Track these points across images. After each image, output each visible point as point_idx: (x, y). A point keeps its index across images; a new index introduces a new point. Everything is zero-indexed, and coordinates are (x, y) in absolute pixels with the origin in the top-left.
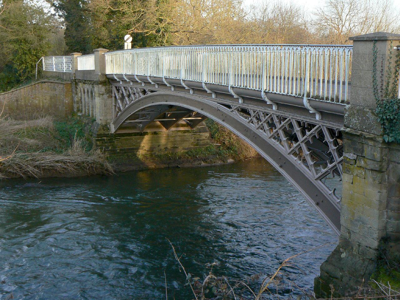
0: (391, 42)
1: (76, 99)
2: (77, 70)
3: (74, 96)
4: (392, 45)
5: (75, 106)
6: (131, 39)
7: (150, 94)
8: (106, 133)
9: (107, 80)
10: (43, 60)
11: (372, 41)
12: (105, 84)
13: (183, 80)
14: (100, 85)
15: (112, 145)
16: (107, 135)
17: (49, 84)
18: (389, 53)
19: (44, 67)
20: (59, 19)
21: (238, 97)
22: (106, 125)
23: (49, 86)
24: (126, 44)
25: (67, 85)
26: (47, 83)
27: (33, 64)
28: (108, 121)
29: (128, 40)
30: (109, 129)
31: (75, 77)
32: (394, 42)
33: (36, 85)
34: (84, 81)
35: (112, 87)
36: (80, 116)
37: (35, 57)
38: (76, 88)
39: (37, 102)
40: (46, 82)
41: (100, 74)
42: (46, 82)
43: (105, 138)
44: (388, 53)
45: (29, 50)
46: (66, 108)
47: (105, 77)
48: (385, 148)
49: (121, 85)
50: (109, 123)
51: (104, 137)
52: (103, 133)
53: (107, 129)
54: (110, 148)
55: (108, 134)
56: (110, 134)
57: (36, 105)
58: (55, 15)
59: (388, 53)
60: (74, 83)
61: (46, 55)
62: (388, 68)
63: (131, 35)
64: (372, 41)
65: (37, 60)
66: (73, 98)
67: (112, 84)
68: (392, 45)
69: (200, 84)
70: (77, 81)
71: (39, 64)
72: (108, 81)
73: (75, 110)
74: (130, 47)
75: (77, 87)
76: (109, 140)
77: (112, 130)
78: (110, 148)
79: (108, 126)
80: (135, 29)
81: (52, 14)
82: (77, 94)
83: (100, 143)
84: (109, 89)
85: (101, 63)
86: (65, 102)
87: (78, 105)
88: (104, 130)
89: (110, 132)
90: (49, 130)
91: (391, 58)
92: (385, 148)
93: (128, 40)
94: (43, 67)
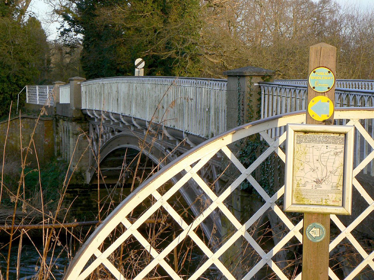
0: (251, 78)
1: (56, 140)
2: (58, 103)
3: (54, 135)
4: (252, 81)
5: (56, 148)
6: (143, 64)
7: (117, 133)
8: (80, 183)
9: (83, 116)
10: (27, 90)
11: (236, 76)
12: (80, 121)
13: (133, 118)
14: (74, 123)
15: (87, 199)
16: (80, 185)
17: (29, 120)
18: (249, 90)
19: (27, 99)
20: (75, 35)
21: (175, 139)
22: (80, 173)
23: (28, 122)
24: (136, 70)
25: (47, 122)
26: (26, 119)
27: (13, 95)
28: (84, 168)
29: (140, 64)
30: (83, 178)
31: (56, 112)
32: (254, 79)
33: (14, 122)
34: (62, 117)
35: (89, 126)
36: (58, 162)
37: (15, 86)
38: (57, 126)
39: (13, 143)
40: (25, 118)
41: (74, 108)
42: (25, 118)
43: (78, 190)
44: (247, 90)
45: (8, 77)
46: (45, 151)
47: (80, 112)
48: (247, 197)
49: (96, 122)
50: (85, 171)
51: (76, 188)
52: (75, 183)
53: (81, 178)
54: (84, 202)
55: (82, 185)
56: (84, 184)
57: (12, 146)
58: (69, 30)
59: (247, 90)
60: (55, 119)
61: (31, 82)
62: (248, 106)
63: (144, 59)
64: (236, 76)
65: (18, 89)
66: (53, 139)
67: (89, 122)
68: (252, 81)
69: (144, 122)
70: (57, 117)
71: (21, 94)
72: (85, 117)
73: (56, 154)
74: (142, 74)
75: (58, 124)
76: (83, 192)
77: (87, 180)
78: (84, 202)
79: (83, 174)
80: (151, 51)
81: (65, 30)
82: (57, 133)
83: (71, 196)
84: (86, 128)
85: (77, 95)
86: (45, 143)
87: (59, 147)
88: (77, 179)
89: (85, 182)
90: (12, 177)
91: (251, 95)
92: (247, 197)
93: (140, 64)
94: (26, 99)
